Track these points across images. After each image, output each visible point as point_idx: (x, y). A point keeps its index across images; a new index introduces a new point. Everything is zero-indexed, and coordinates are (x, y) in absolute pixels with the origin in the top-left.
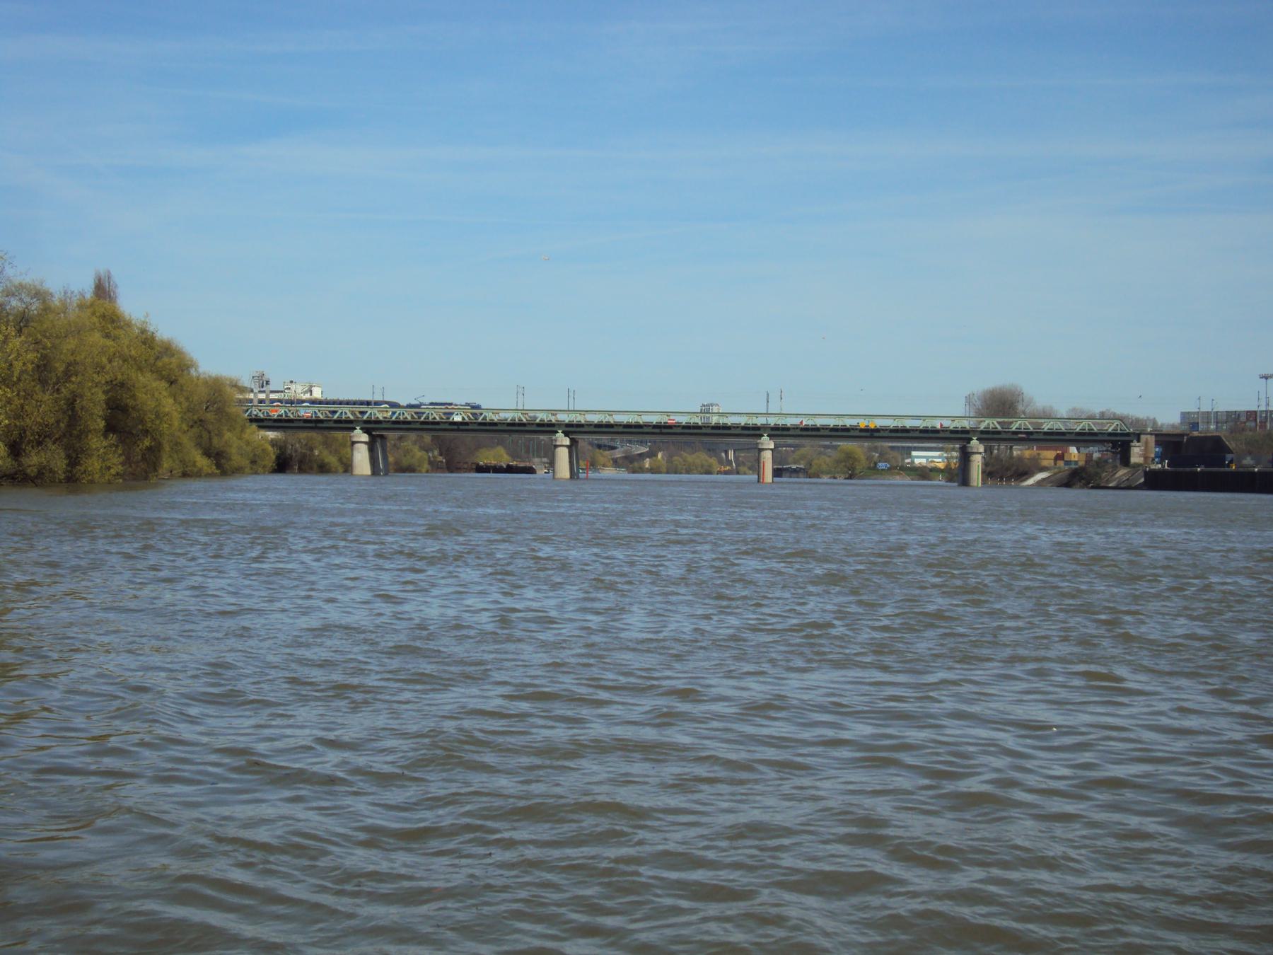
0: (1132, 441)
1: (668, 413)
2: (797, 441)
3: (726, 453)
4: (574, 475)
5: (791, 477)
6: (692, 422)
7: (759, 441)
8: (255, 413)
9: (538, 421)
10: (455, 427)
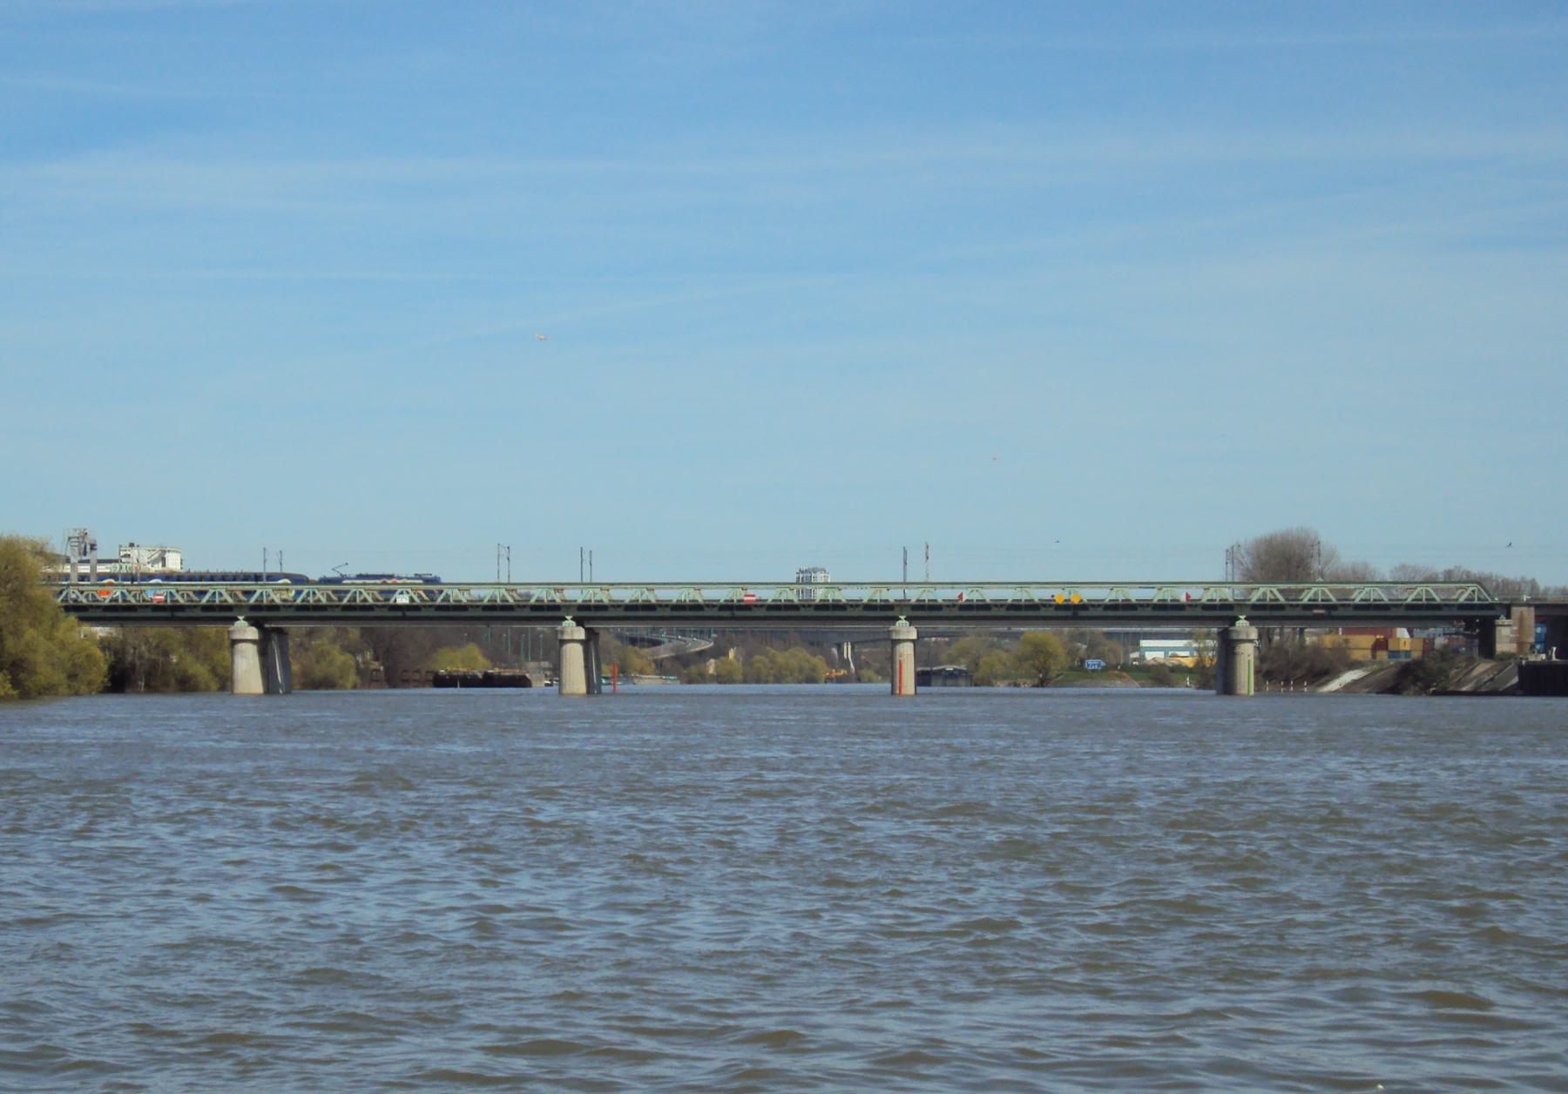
0: (1498, 617)
1: (743, 585)
2: (953, 627)
3: (840, 647)
4: (592, 688)
5: (945, 685)
6: (783, 598)
7: (892, 628)
8: (74, 596)
9: (533, 601)
10: (399, 614)
